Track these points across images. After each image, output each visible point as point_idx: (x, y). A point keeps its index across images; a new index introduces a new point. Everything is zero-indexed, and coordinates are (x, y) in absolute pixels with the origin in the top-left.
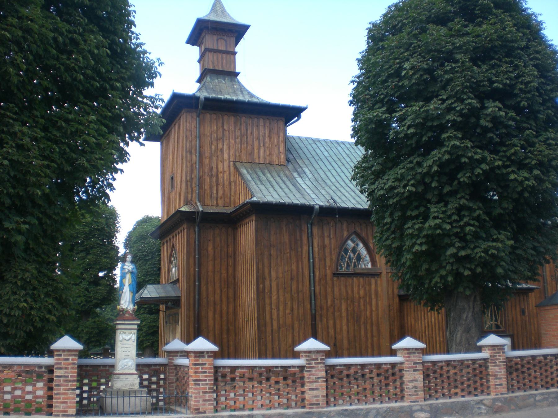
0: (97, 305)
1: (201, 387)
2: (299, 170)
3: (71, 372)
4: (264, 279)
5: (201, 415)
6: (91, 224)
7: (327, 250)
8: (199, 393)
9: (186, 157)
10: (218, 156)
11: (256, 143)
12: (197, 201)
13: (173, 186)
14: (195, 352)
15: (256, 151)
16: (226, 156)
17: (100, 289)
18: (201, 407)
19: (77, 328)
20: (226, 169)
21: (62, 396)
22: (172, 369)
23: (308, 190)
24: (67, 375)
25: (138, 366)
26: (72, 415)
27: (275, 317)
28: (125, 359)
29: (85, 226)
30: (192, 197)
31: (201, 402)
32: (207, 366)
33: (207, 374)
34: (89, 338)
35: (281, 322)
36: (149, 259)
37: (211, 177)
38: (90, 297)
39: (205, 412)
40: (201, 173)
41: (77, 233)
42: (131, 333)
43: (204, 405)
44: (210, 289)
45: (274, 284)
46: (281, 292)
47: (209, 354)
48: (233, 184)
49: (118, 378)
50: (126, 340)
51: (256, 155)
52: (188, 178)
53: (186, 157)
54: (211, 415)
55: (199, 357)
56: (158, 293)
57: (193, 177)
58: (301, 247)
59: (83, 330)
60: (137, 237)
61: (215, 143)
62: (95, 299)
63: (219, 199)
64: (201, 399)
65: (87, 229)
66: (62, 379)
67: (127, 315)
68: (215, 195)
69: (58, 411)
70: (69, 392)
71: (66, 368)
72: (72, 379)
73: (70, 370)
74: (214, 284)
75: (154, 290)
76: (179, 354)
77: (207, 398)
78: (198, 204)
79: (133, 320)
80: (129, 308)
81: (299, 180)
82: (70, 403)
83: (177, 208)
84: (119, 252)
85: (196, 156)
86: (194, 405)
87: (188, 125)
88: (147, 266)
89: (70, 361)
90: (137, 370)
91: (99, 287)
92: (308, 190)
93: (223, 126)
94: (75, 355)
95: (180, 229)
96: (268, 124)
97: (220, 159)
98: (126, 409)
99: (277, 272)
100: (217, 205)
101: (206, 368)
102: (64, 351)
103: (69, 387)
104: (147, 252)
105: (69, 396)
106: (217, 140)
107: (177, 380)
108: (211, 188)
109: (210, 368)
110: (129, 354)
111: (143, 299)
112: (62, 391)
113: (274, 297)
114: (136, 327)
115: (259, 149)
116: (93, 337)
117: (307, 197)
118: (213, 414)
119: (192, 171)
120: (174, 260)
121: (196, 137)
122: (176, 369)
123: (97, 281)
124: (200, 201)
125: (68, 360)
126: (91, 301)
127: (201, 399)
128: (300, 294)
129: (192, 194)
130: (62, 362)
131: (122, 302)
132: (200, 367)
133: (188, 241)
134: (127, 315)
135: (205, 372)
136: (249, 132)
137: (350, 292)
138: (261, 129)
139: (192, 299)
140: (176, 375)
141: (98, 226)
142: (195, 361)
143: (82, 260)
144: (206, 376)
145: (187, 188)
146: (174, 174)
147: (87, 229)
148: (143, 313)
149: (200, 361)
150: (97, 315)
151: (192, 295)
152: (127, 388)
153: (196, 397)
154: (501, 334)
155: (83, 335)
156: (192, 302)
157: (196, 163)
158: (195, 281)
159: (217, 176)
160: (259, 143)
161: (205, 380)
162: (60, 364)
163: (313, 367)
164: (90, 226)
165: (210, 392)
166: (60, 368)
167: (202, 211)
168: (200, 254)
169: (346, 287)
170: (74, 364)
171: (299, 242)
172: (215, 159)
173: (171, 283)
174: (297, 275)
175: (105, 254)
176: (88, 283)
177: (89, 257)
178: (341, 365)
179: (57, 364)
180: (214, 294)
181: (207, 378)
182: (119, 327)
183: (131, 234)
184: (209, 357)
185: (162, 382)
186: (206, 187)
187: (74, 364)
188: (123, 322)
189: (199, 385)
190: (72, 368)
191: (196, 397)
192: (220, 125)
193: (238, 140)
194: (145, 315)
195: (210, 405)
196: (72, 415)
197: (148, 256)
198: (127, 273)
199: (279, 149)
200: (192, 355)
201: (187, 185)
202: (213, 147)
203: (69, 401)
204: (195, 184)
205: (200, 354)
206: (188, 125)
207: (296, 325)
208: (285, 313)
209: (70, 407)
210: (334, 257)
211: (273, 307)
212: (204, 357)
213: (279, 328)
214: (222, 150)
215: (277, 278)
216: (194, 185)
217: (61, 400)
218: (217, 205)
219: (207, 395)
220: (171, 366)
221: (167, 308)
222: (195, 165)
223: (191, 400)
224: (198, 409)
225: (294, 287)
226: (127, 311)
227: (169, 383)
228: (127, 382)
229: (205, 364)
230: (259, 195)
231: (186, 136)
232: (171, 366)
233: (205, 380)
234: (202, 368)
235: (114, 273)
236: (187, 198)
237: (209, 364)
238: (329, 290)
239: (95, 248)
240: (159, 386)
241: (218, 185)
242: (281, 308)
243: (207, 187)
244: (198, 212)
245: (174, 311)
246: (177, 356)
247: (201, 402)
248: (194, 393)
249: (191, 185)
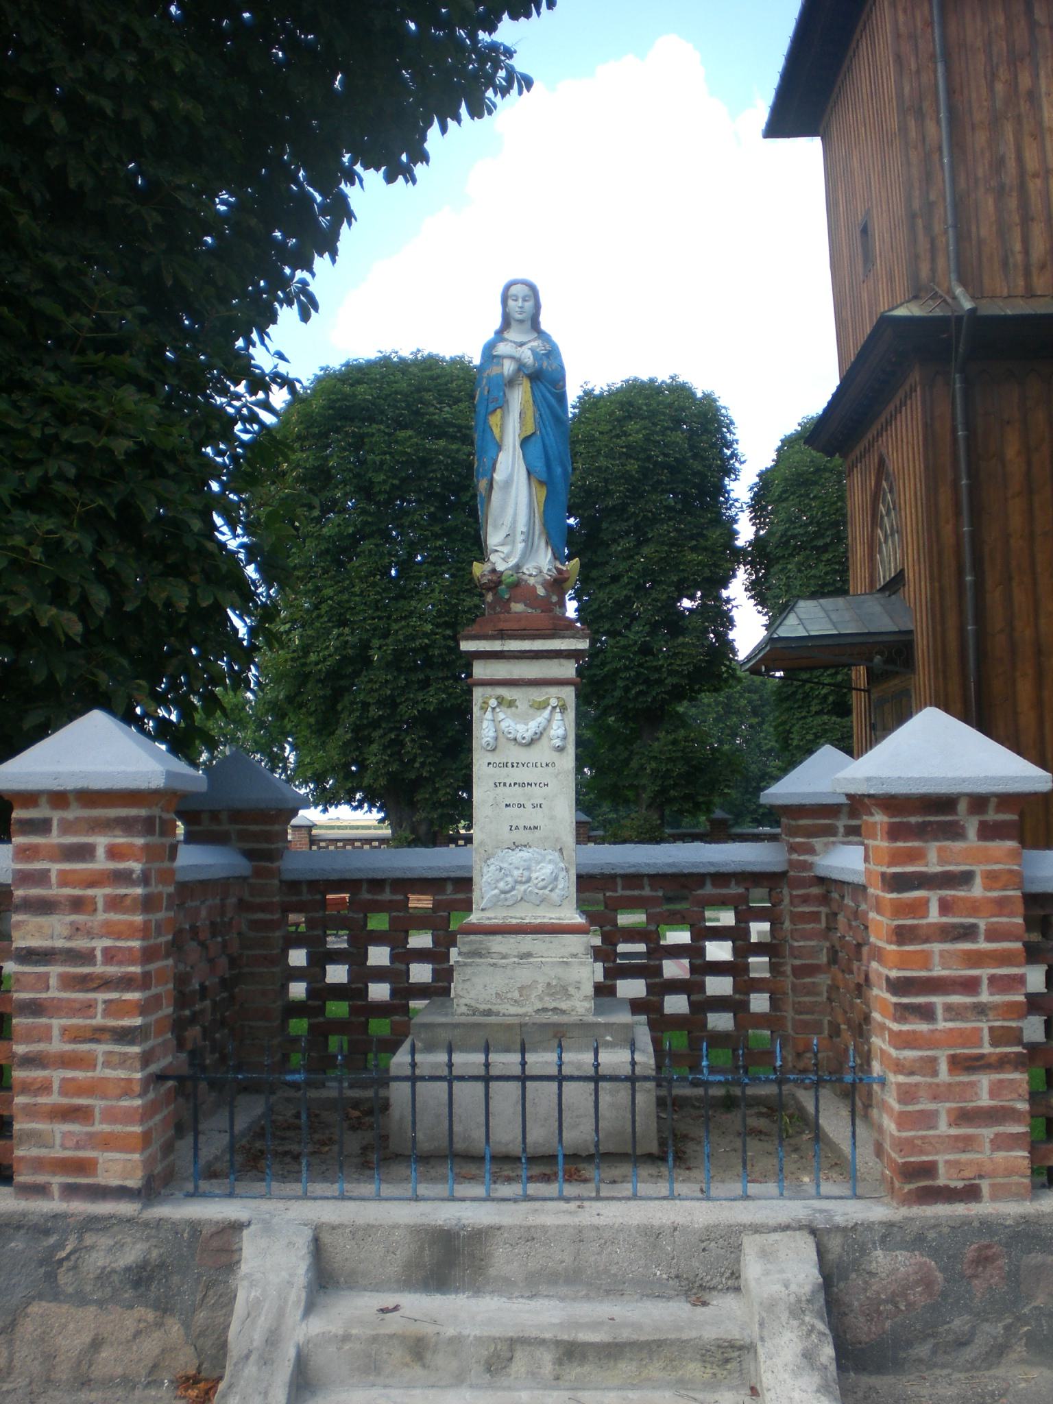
0: (678, 694)
1: (942, 1025)
3: (110, 930)
5: (942, 1210)
6: (645, 450)
8: (930, 1066)
9: (903, 129)
10: (1019, 119)
12: (954, 283)
13: (868, 258)
14: (892, 803)
17: (684, 645)
18: (941, 1159)
19: (627, 762)
21: (57, 1076)
22: (805, 899)
24: (80, 943)
25: (587, 882)
26: (122, 1193)
28: (515, 846)
29: (628, 456)
30: (933, 270)
31: (944, 1128)
32: (977, 890)
33: (983, 945)
34: (663, 791)
36: (826, 546)
37: (1000, 193)
38: (658, 669)
39: (971, 1193)
40: (962, 184)
41: (606, 481)
42: (542, 706)
43: (966, 1143)
44: (1020, 597)
47: (992, 816)
49: (476, 954)
50: (526, 750)
52: (916, 204)
53: (903, 129)
54: (1012, 1209)
55: (921, 832)
56: (834, 625)
57: (932, 197)
59: (642, 768)
60: (786, 479)
61: (1003, 73)
62: (671, 673)
63: (1035, 271)
64: (944, 1108)
65: (633, 466)
66: (54, 971)
67: (518, 607)
68: (1019, 258)
69: (39, 1165)
70: (100, 1049)
71: (78, 905)
72: (113, 970)
73: (101, 916)
74: (1035, 583)
75: (822, 614)
77: (985, 1100)
78: (959, 291)
80: (529, 569)
82: (111, 1116)
83: (883, 307)
84: (737, 533)
85: (938, 122)
86: (903, 1145)
87: (901, 18)
88: (821, 566)
89: (101, 863)
90: (581, 904)
91: (681, 640)
94: (126, 825)
95: (901, 394)
98: (506, 1135)
100: (1030, 294)
101: (974, 907)
102: (59, 799)
103: (99, 1020)
104: (819, 524)
105: (101, 1072)
106: (1014, 61)
107: (834, 958)
108: (1002, 232)
109: (1001, 905)
110: (536, 818)
111: (779, 645)
112: (57, 1046)
114: (568, 669)
116: (675, 786)
118: (1028, 1207)
119: (928, 177)
120: (888, 514)
121: (933, 56)
122: (825, 899)
123: (675, 623)
124: (963, 282)
125: (83, 852)
126: (660, 682)
127: (944, 1108)
129: (933, 260)
130: (55, 867)
131: (494, 539)
132: (933, 897)
133: (928, 427)
134: (518, 607)
135: (968, 933)
139: (952, 635)
140: (829, 929)
141: (666, 455)
142: (895, 858)
143: (625, 559)
144: (976, 959)
145: (913, 240)
146: (868, 213)
147: (633, 466)
148: (817, 713)
149: (933, 856)
150: (682, 721)
151: (952, 621)
152: (528, 1009)
153: (907, 1095)
155: (644, 781)
156: (953, 646)
157: (940, 149)
158: (960, 573)
159: (1022, 187)
161: (970, 986)
162: (41, 878)
164: (642, 456)
165: (1001, 1063)
166: (45, 907)
167: (973, 311)
168: (973, 475)
170: (122, 877)
173: (882, 590)
175: (692, 538)
176: (647, 628)
177: (646, 550)
179: (25, 878)
180: (1037, 616)
181: (984, 973)
182: (481, 670)
183: (766, 478)
184: (988, 832)
185: (759, 964)
186: (984, 232)
187: (122, 877)
188: (496, 646)
189: (926, 1013)
190: (114, 904)
191: (907, 1095)
194: (826, 718)
195: (1000, 1143)
197: (822, 536)
198: (511, 383)
200: (880, 818)
201: (912, 229)
202: (999, 87)
203: (98, 1104)
204: (943, 215)
205: (926, 813)
206: (901, 18)
209: (107, 1142)
212: (954, 832)
216: (938, 228)
217: (55, 1099)
218: (1030, 294)
219: (985, 1081)
220: (802, 883)
221: (873, 677)
222: (936, 157)
223: (884, 1105)
224: (929, 1170)
226: (517, 586)
227: (799, 971)
228: (524, 975)
229: (965, 879)
231: (898, 58)
232: (802, 883)
233: (970, 986)
234: (945, 907)
235: (725, 593)
236: (914, 276)
237: (992, 878)
239: (662, 521)
240: (746, 985)
241: (1026, 220)
243: (985, 230)
244: (959, 319)
245: (894, 684)
246: (830, 831)
247: (944, 1128)
248: (899, 1067)
249: (928, 228)
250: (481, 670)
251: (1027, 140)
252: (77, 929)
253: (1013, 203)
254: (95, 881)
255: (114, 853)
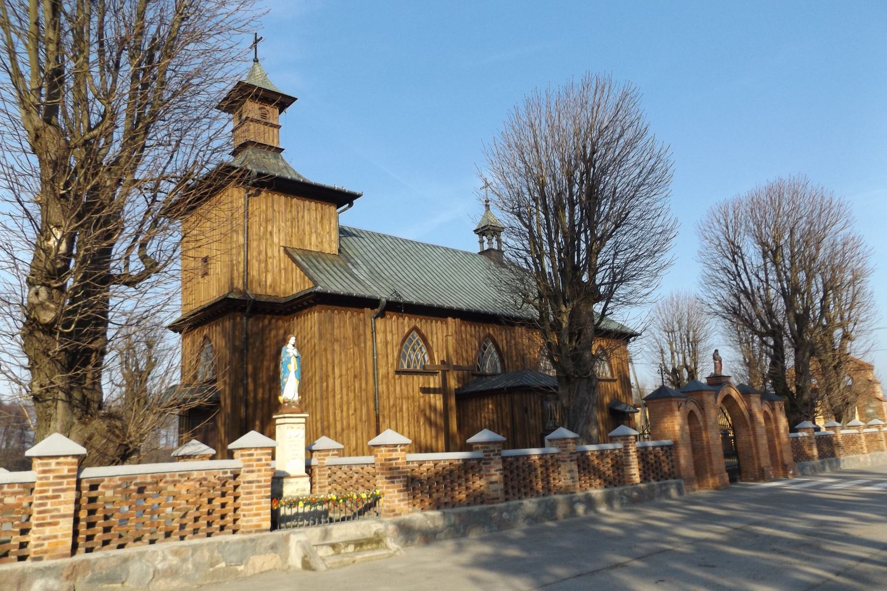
2: (352, 261)
3: (265, 476)
4: (327, 376)
7: (389, 347)
10: (267, 239)
11: (307, 228)
15: (307, 237)
16: (276, 240)
20: (276, 254)
21: (254, 507)
23: (367, 282)
24: (259, 479)
26: (266, 530)
27: (338, 418)
31: (397, 503)
35: (345, 423)
37: (260, 262)
39: (39, 559)
45: (338, 382)
46: (344, 390)
48: (283, 272)
51: (307, 242)
58: (365, 343)
61: (264, 224)
66: (254, 485)
71: (259, 471)
76: (331, 453)
79: (302, 412)
81: (354, 270)
82: (265, 514)
92: (367, 282)
93: (273, 206)
96: (320, 209)
97: (269, 242)
99: (341, 370)
106: (267, 221)
112: (255, 500)
113: (338, 397)
114: (303, 420)
115: (310, 235)
117: (370, 289)
125: (260, 460)
128: (363, 393)
136: (300, 215)
137: (411, 391)
138: (313, 213)
154: (571, 428)
159: (266, 261)
160: (311, 228)
162: (252, 466)
163: (491, 459)
169: (407, 385)
171: (362, 338)
172: (264, 242)
174: (360, 372)
178: (511, 457)
190: (266, 470)
192: (270, 204)
193: (289, 223)
196: (266, 530)
199: (330, 236)
207: (359, 428)
208: (348, 413)
209: (263, 520)
210: (396, 354)
211: (337, 406)
213: (343, 430)
214: (271, 233)
215: (341, 376)
225: (357, 385)
230: (323, 284)
238: (391, 389)
242: (345, 409)
250: (278, 421)
251: (269, 246)
252: (259, 476)
253: (263, 265)
254: (262, 466)
255: (266, 460)
